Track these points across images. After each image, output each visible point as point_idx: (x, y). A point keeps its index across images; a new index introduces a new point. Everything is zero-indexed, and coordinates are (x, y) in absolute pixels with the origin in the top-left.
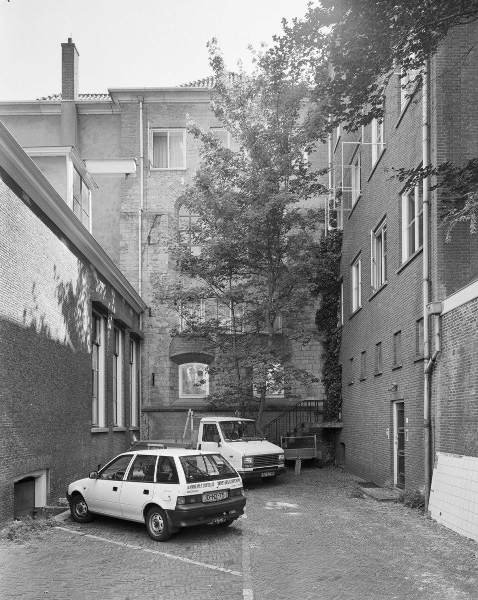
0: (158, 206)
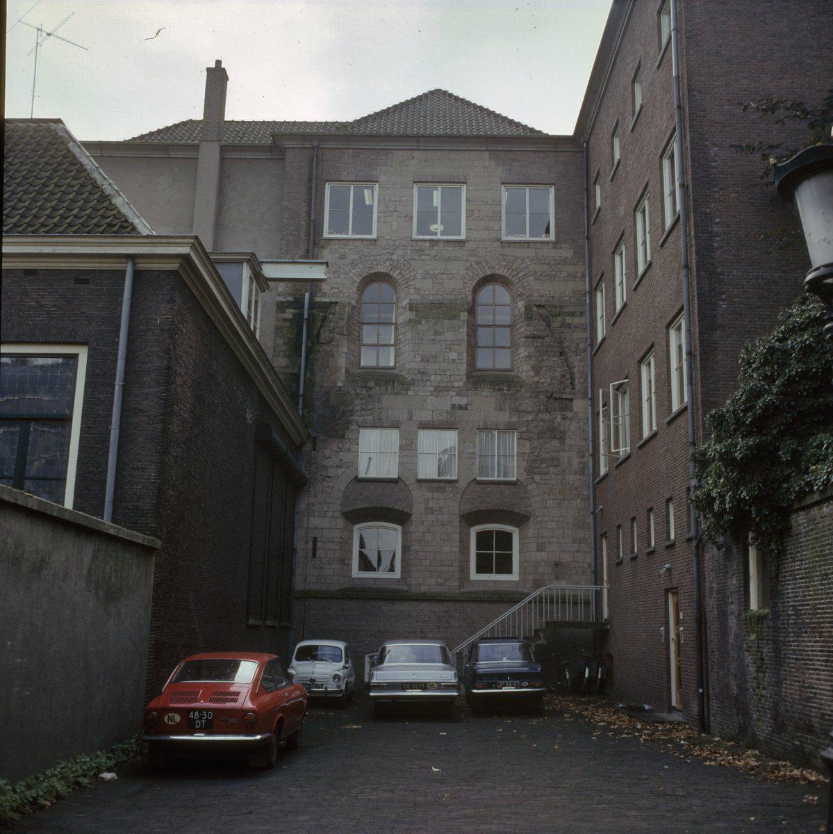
0: (332, 288)
